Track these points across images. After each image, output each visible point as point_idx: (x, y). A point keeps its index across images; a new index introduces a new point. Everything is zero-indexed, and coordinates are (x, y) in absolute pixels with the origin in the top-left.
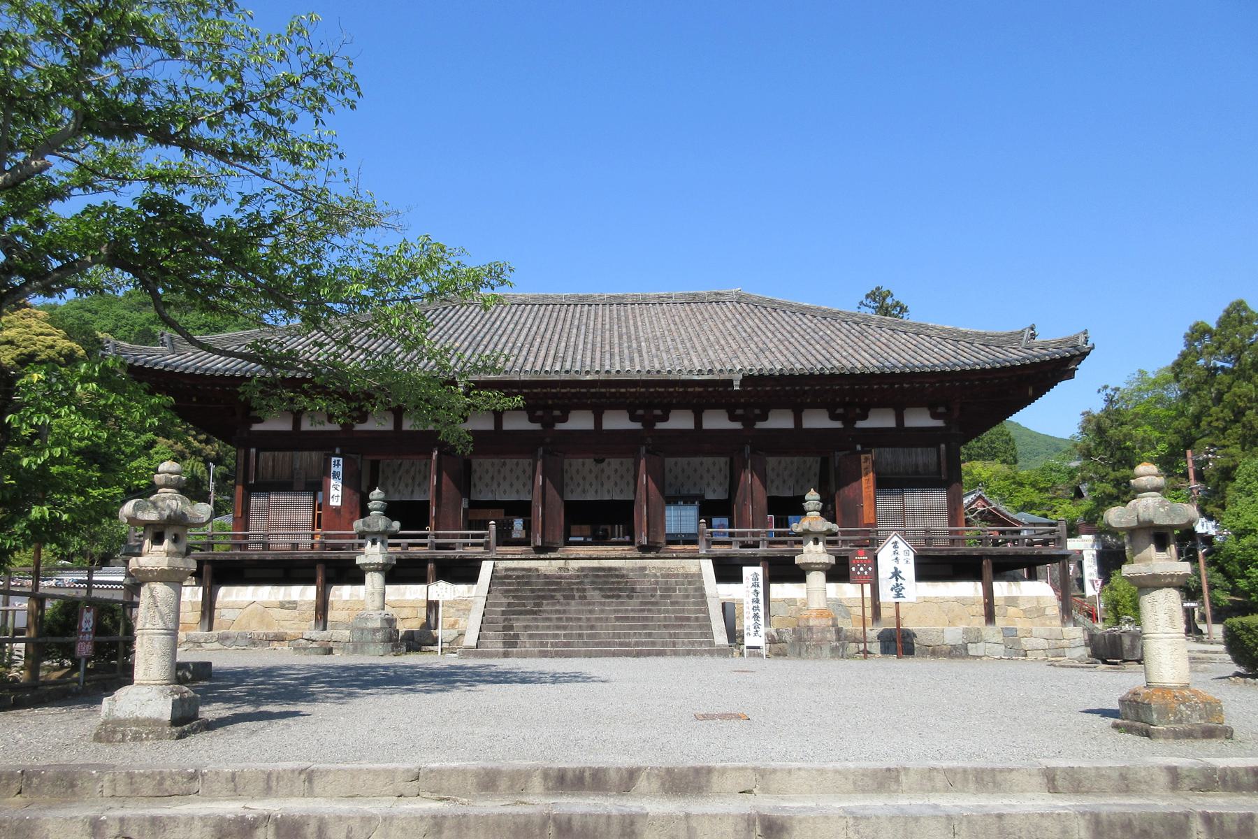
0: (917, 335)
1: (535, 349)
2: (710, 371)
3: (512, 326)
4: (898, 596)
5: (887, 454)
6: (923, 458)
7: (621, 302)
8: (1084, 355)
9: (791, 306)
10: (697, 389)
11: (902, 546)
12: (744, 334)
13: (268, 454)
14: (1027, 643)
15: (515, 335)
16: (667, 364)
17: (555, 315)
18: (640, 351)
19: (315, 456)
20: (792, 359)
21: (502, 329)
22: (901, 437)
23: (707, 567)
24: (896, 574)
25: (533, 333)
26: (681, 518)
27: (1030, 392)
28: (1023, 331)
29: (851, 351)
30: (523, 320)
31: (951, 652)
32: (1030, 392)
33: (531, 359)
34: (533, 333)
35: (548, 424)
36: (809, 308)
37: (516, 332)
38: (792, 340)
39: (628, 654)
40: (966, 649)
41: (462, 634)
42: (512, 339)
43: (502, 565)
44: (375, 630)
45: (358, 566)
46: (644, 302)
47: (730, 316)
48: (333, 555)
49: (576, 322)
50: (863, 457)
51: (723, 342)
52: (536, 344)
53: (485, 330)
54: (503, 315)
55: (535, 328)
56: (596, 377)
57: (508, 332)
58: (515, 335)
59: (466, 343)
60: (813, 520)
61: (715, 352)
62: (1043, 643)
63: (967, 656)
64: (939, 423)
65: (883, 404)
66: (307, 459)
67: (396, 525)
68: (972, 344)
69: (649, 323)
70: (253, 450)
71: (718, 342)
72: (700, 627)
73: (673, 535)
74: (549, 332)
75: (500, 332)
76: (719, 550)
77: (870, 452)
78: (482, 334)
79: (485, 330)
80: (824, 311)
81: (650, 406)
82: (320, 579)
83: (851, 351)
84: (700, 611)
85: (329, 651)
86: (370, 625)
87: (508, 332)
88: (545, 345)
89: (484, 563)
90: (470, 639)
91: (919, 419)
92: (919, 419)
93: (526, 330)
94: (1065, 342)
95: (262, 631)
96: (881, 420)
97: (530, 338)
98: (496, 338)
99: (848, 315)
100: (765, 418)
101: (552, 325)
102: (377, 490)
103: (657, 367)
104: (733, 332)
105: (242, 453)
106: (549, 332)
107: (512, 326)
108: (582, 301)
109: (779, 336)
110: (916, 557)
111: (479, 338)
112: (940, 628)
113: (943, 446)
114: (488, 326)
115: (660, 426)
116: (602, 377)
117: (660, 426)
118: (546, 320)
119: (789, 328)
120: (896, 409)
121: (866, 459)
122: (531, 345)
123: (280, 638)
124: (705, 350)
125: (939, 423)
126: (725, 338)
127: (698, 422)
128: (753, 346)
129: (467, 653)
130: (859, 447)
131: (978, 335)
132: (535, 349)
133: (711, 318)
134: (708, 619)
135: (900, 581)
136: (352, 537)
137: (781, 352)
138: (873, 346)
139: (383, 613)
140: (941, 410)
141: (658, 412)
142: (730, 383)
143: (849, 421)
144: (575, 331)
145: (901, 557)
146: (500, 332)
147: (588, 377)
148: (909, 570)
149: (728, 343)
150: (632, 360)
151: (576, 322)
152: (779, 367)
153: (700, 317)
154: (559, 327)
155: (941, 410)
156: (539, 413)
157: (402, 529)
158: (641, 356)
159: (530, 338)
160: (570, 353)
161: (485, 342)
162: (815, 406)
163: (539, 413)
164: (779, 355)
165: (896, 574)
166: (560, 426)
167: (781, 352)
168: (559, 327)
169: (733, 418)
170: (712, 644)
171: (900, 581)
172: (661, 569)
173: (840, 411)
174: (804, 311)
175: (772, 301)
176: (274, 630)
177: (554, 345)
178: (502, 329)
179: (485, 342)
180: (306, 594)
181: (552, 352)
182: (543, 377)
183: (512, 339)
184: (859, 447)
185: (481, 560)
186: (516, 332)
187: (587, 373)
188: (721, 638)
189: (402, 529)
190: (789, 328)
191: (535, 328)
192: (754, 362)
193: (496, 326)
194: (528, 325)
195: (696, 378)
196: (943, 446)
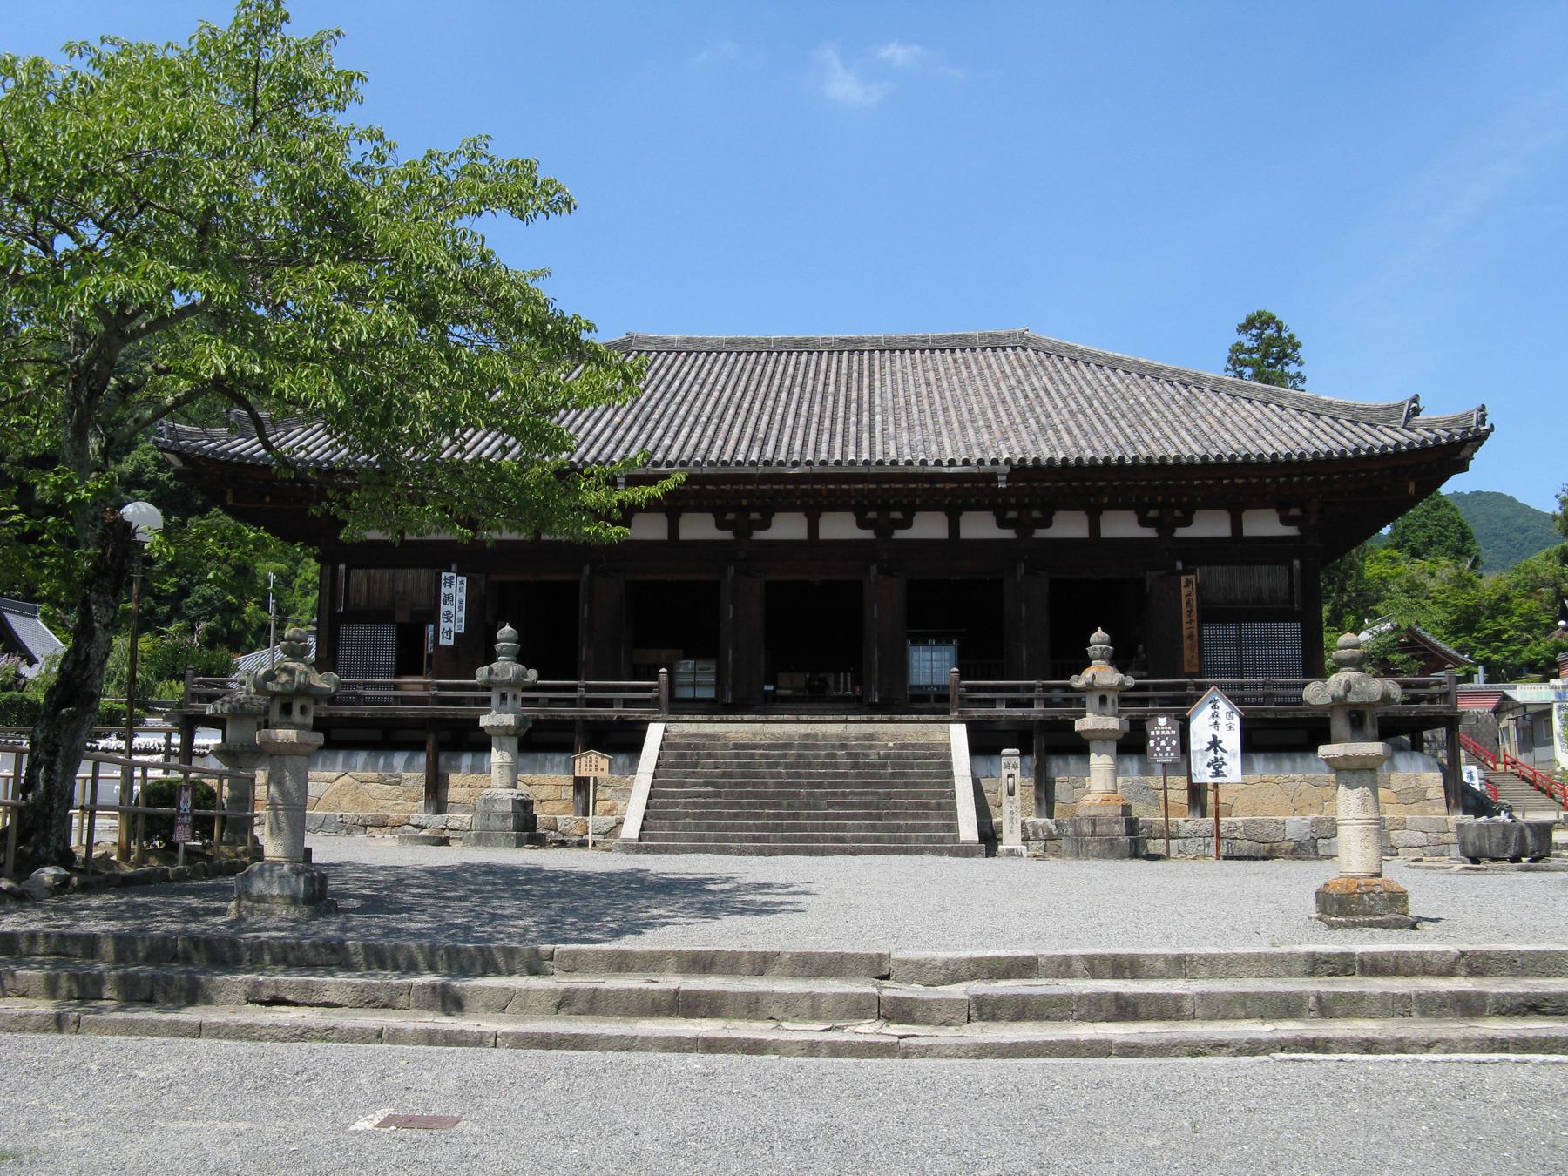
0: (1266, 404)
1: (725, 427)
2: (966, 462)
3: (696, 388)
4: (1217, 774)
5: (1219, 576)
6: (1269, 580)
7: (854, 347)
8: (1480, 438)
9: (1097, 356)
10: (948, 486)
11: (1223, 707)
12: (1023, 402)
13: (361, 572)
14: (1397, 837)
15: (699, 404)
16: (906, 450)
17: (759, 368)
18: (872, 428)
19: (424, 575)
20: (1083, 443)
21: (682, 393)
22: (1237, 550)
23: (958, 736)
24: (1215, 744)
25: (724, 399)
26: (932, 664)
27: (1412, 488)
28: (1403, 404)
29: (1167, 430)
30: (712, 379)
31: (1294, 850)
32: (1412, 488)
33: (719, 442)
34: (724, 399)
35: (743, 529)
36: (1120, 360)
37: (702, 397)
38: (1089, 411)
39: (843, 852)
40: (1315, 847)
41: (620, 823)
42: (695, 410)
43: (676, 729)
44: (504, 817)
45: (482, 729)
46: (887, 347)
47: (1008, 371)
48: (450, 711)
49: (788, 382)
50: (1183, 579)
51: (990, 415)
52: (728, 418)
53: (658, 395)
54: (685, 369)
55: (728, 392)
56: (806, 470)
57: (690, 398)
58: (699, 404)
59: (631, 417)
60: (1101, 673)
61: (977, 432)
62: (1417, 837)
63: (1317, 854)
64: (1291, 531)
65: (1211, 503)
66: (411, 579)
67: (533, 674)
68: (1336, 420)
69: (895, 381)
70: (342, 567)
71: (983, 413)
72: (942, 817)
73: (920, 687)
74: (748, 398)
75: (679, 398)
76: (978, 712)
77: (1192, 572)
78: (652, 402)
79: (658, 395)
80: (1142, 365)
81: (884, 508)
82: (429, 747)
83: (1167, 430)
84: (942, 795)
85: (445, 842)
86: (498, 808)
87: (690, 398)
88: (740, 419)
89: (651, 726)
90: (631, 830)
91: (1263, 525)
92: (1263, 525)
93: (716, 394)
94: (1454, 421)
95: (352, 814)
96: (1210, 525)
97: (720, 408)
98: (673, 408)
99: (1175, 372)
100: (1187, 522)
101: (752, 387)
102: (508, 628)
103: (893, 454)
104: (1009, 399)
105: (328, 570)
106: (748, 398)
107: (696, 388)
108: (799, 346)
109: (1073, 405)
110: (1242, 720)
111: (648, 409)
112: (1280, 818)
113: (1296, 563)
114: (662, 388)
115: (900, 534)
116: (816, 469)
117: (900, 534)
118: (745, 378)
119: (1088, 392)
120: (1279, 510)
121: (1188, 582)
122: (721, 419)
123: (381, 824)
124: (963, 428)
125: (1291, 531)
126: (994, 407)
127: (1237, 525)
128: (1032, 421)
129: (628, 848)
130: (1179, 565)
131: (1348, 408)
132: (725, 427)
133: (981, 374)
134: (953, 807)
135: (1220, 754)
136: (474, 688)
137: (1069, 432)
138: (1199, 422)
139: (516, 792)
140: (1295, 512)
141: (897, 515)
142: (991, 477)
143: (1165, 527)
144: (784, 396)
145: (1223, 721)
146: (679, 398)
147: (796, 471)
148: (1232, 740)
149: (997, 415)
150: (858, 443)
151: (788, 382)
152: (1062, 455)
153: (965, 373)
154: (763, 389)
155: (1295, 512)
156: (731, 516)
157: (540, 678)
158: (872, 437)
159: (720, 408)
160: (774, 432)
161: (656, 416)
162: (1262, 504)
163: (731, 516)
164: (1065, 436)
165: (1215, 744)
166: (759, 535)
167: (1069, 432)
168: (763, 389)
169: (1144, 522)
170: (956, 838)
171: (1220, 754)
172: (893, 737)
173: (1153, 513)
174: (1114, 364)
175: (1071, 349)
176: (368, 813)
177: (753, 419)
178: (682, 393)
179: (656, 416)
180: (411, 772)
181: (749, 431)
182: (733, 469)
183: (695, 410)
184: (1179, 565)
185: (647, 722)
186: (702, 397)
187: (795, 464)
188: (968, 830)
189: (540, 678)
190: (1088, 392)
191: (728, 392)
192: (1029, 446)
193: (673, 389)
194: (719, 387)
195: (945, 470)
196: (1296, 563)
